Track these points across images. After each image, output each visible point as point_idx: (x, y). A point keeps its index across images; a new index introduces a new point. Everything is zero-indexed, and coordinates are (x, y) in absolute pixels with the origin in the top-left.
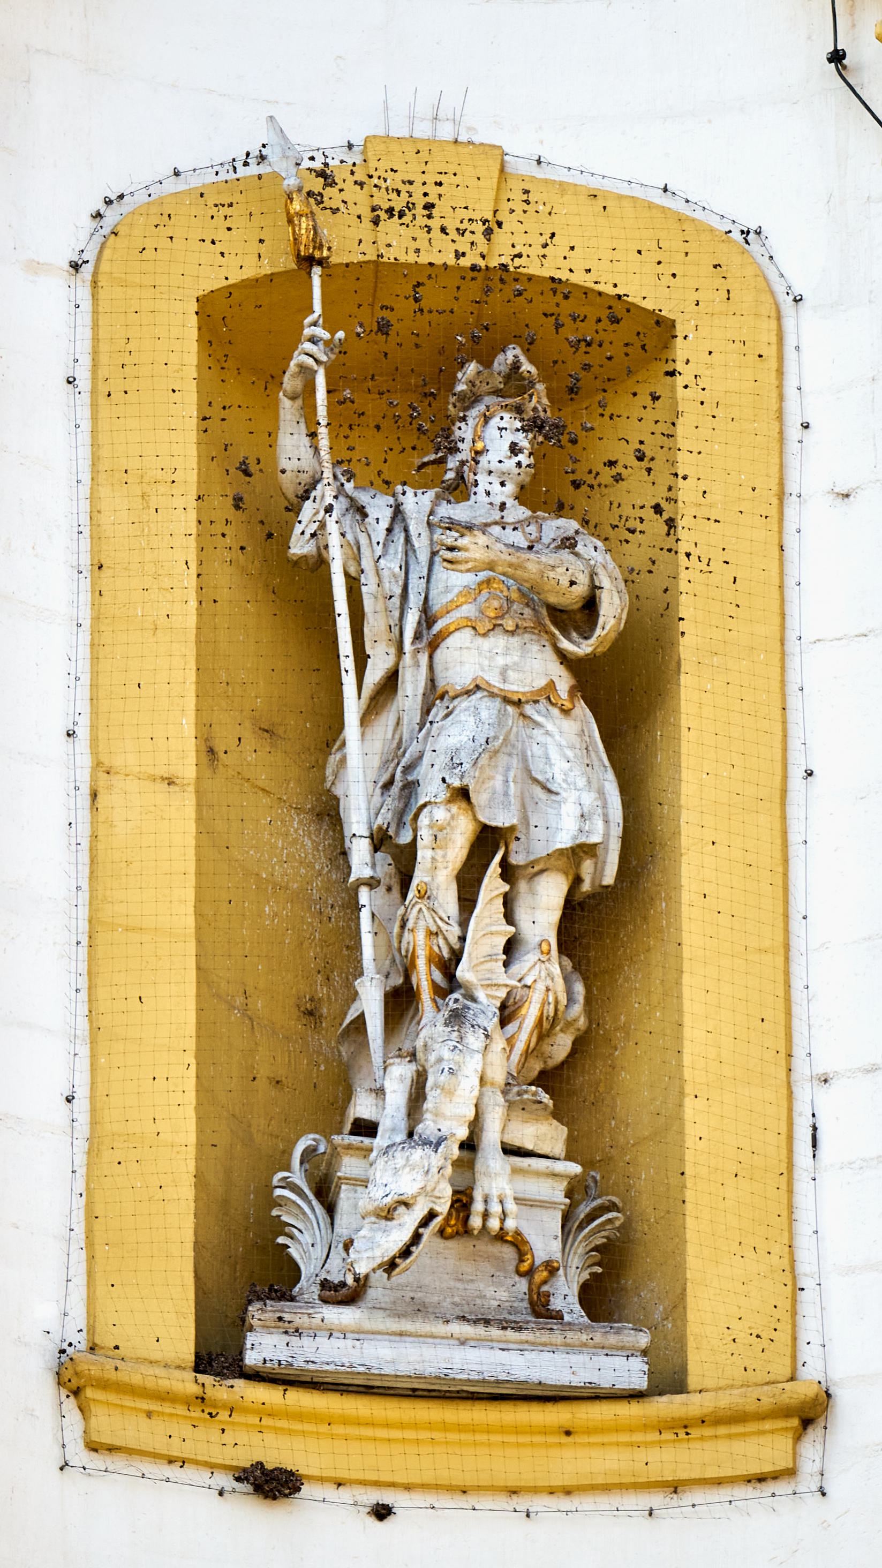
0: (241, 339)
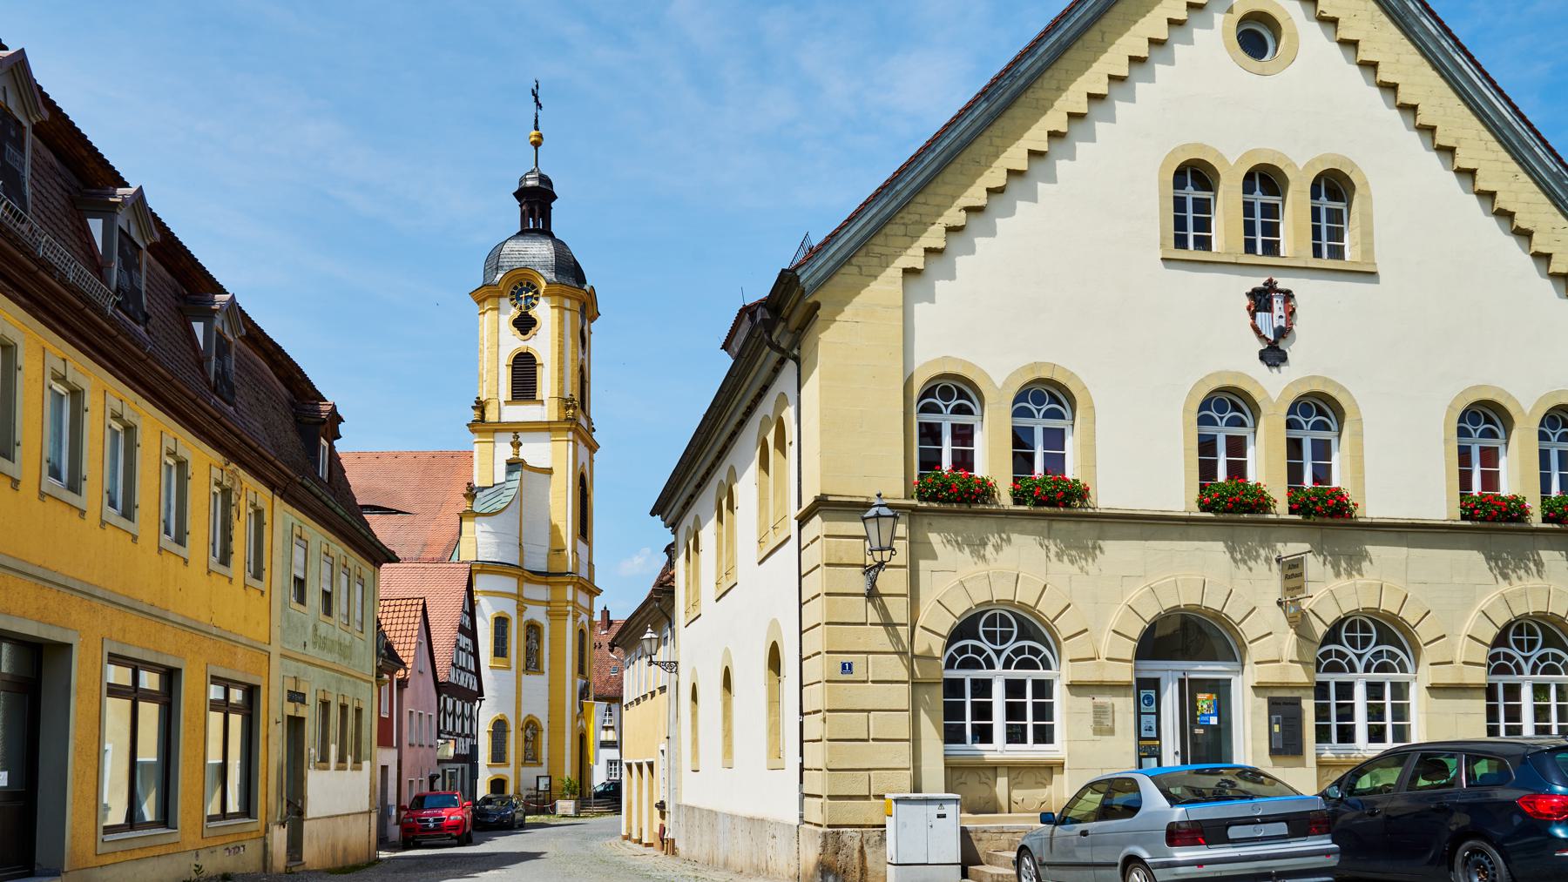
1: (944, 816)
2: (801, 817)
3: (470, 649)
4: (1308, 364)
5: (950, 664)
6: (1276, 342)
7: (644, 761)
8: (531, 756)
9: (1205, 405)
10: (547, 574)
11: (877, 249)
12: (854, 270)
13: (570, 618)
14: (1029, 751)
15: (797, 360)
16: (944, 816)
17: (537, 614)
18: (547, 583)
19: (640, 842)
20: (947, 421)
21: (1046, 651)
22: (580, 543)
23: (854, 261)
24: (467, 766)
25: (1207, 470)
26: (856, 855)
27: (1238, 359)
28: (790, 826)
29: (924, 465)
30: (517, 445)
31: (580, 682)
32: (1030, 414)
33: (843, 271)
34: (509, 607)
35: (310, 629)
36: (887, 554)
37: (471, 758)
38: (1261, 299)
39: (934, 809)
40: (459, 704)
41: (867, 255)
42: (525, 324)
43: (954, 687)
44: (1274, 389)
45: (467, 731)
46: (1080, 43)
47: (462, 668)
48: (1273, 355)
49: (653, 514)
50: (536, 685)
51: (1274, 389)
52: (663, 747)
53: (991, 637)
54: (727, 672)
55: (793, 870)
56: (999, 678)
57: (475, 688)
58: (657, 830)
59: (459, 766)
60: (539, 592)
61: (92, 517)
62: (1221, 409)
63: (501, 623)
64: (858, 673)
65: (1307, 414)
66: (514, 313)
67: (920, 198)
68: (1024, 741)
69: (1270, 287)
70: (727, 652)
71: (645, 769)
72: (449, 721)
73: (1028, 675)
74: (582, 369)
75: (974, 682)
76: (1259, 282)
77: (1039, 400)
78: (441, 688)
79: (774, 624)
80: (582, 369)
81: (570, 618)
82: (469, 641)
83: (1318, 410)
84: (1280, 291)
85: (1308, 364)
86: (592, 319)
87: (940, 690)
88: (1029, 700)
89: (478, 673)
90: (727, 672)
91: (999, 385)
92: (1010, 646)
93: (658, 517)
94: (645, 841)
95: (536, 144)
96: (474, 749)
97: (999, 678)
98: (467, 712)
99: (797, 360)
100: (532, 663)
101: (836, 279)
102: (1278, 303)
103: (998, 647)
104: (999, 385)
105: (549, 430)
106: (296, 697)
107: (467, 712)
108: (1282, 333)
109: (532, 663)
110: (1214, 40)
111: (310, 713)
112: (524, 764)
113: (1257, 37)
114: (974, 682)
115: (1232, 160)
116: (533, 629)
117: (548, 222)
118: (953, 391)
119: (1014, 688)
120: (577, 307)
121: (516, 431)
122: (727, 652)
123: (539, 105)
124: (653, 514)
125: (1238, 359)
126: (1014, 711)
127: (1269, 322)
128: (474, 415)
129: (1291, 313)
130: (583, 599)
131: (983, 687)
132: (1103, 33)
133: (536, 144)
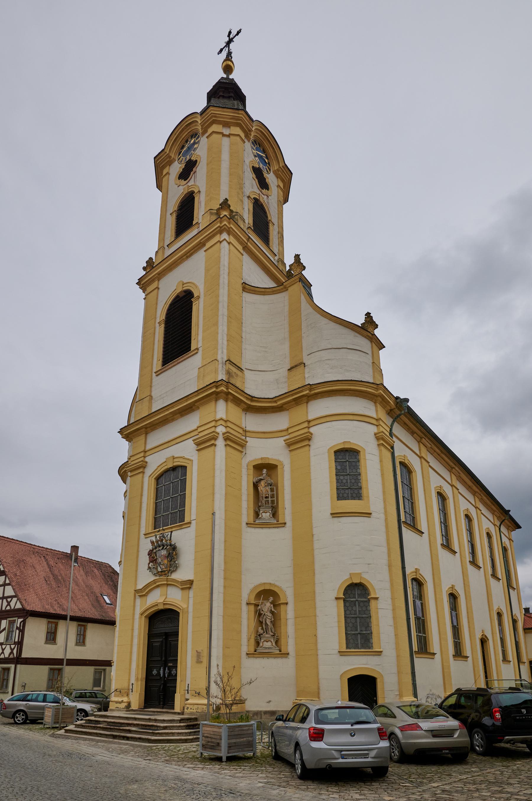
13: (220, 442)
81: (220, 442)
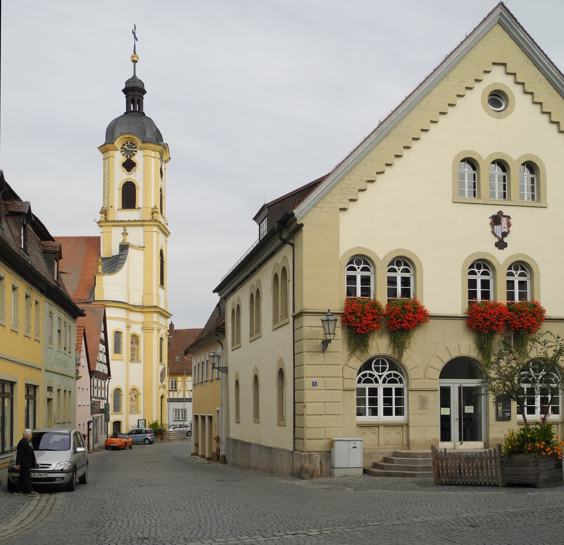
0: (132, 336)
1: (356, 447)
2: (294, 447)
3: (104, 351)
4: (516, 247)
5: (359, 381)
6: (502, 239)
7: (207, 415)
8: (134, 409)
9: (472, 266)
10: (143, 307)
11: (328, 200)
12: (318, 209)
13: (155, 331)
14: (394, 418)
15: (293, 245)
16: (356, 447)
17: (137, 329)
18: (142, 312)
19: (204, 456)
20: (359, 274)
21: (401, 376)
22: (160, 289)
23: (318, 205)
24: (103, 415)
25: (472, 295)
26: (318, 464)
27: (486, 246)
28: (289, 451)
29: (349, 294)
30: (125, 234)
31: (161, 367)
32: (395, 271)
33: (314, 210)
34: (120, 326)
35: (54, 355)
36: (332, 336)
37: (105, 411)
38: (496, 220)
39: (352, 444)
40: (99, 381)
41: (324, 203)
42: (129, 165)
43: (361, 392)
44: (501, 259)
45: (106, 396)
46: (418, 106)
47: (101, 362)
48: (501, 245)
49: (214, 291)
50: (137, 369)
51: (501, 259)
52: (218, 409)
53: (377, 369)
54: (256, 378)
55: (290, 471)
56: (381, 388)
57: (106, 372)
58: (214, 450)
59: (99, 415)
60: (137, 317)
61: (32, 339)
62: (479, 267)
63: (118, 334)
64: (320, 385)
65: (516, 269)
66: (123, 159)
67: (347, 177)
68: (391, 415)
69: (500, 213)
70: (256, 368)
71: (200, 418)
72: (95, 391)
73: (393, 386)
74: (161, 190)
75: (370, 389)
76: (494, 211)
77: (398, 264)
78: (92, 373)
79: (281, 360)
80: (161, 190)
81: (155, 331)
82: (104, 347)
83: (521, 266)
84: (505, 216)
85: (516, 247)
86: (166, 162)
87: (355, 393)
88: (394, 397)
89: (108, 364)
90: (256, 378)
91: (381, 259)
92: (386, 373)
93: (217, 294)
94: (207, 456)
95: (135, 62)
96: (107, 405)
97: (381, 388)
98: (103, 386)
99: (293, 245)
100: (134, 358)
101: (310, 213)
102: (504, 221)
103: (380, 374)
104: (381, 259)
105: (143, 226)
106: (50, 389)
107: (103, 386)
108: (505, 234)
109: (134, 358)
110: (477, 97)
111: (54, 396)
112: (131, 413)
113: (497, 98)
114: (370, 389)
115: (484, 157)
116: (135, 339)
117: (141, 107)
118: (361, 260)
119: (387, 392)
120: (158, 155)
121: (124, 224)
122: (256, 368)
123: (136, 39)
124: (214, 291)
125: (486, 246)
126: (387, 401)
127: (499, 230)
128: (99, 217)
129: (509, 225)
130: (162, 321)
131: (373, 392)
132: (428, 102)
133: (135, 62)
